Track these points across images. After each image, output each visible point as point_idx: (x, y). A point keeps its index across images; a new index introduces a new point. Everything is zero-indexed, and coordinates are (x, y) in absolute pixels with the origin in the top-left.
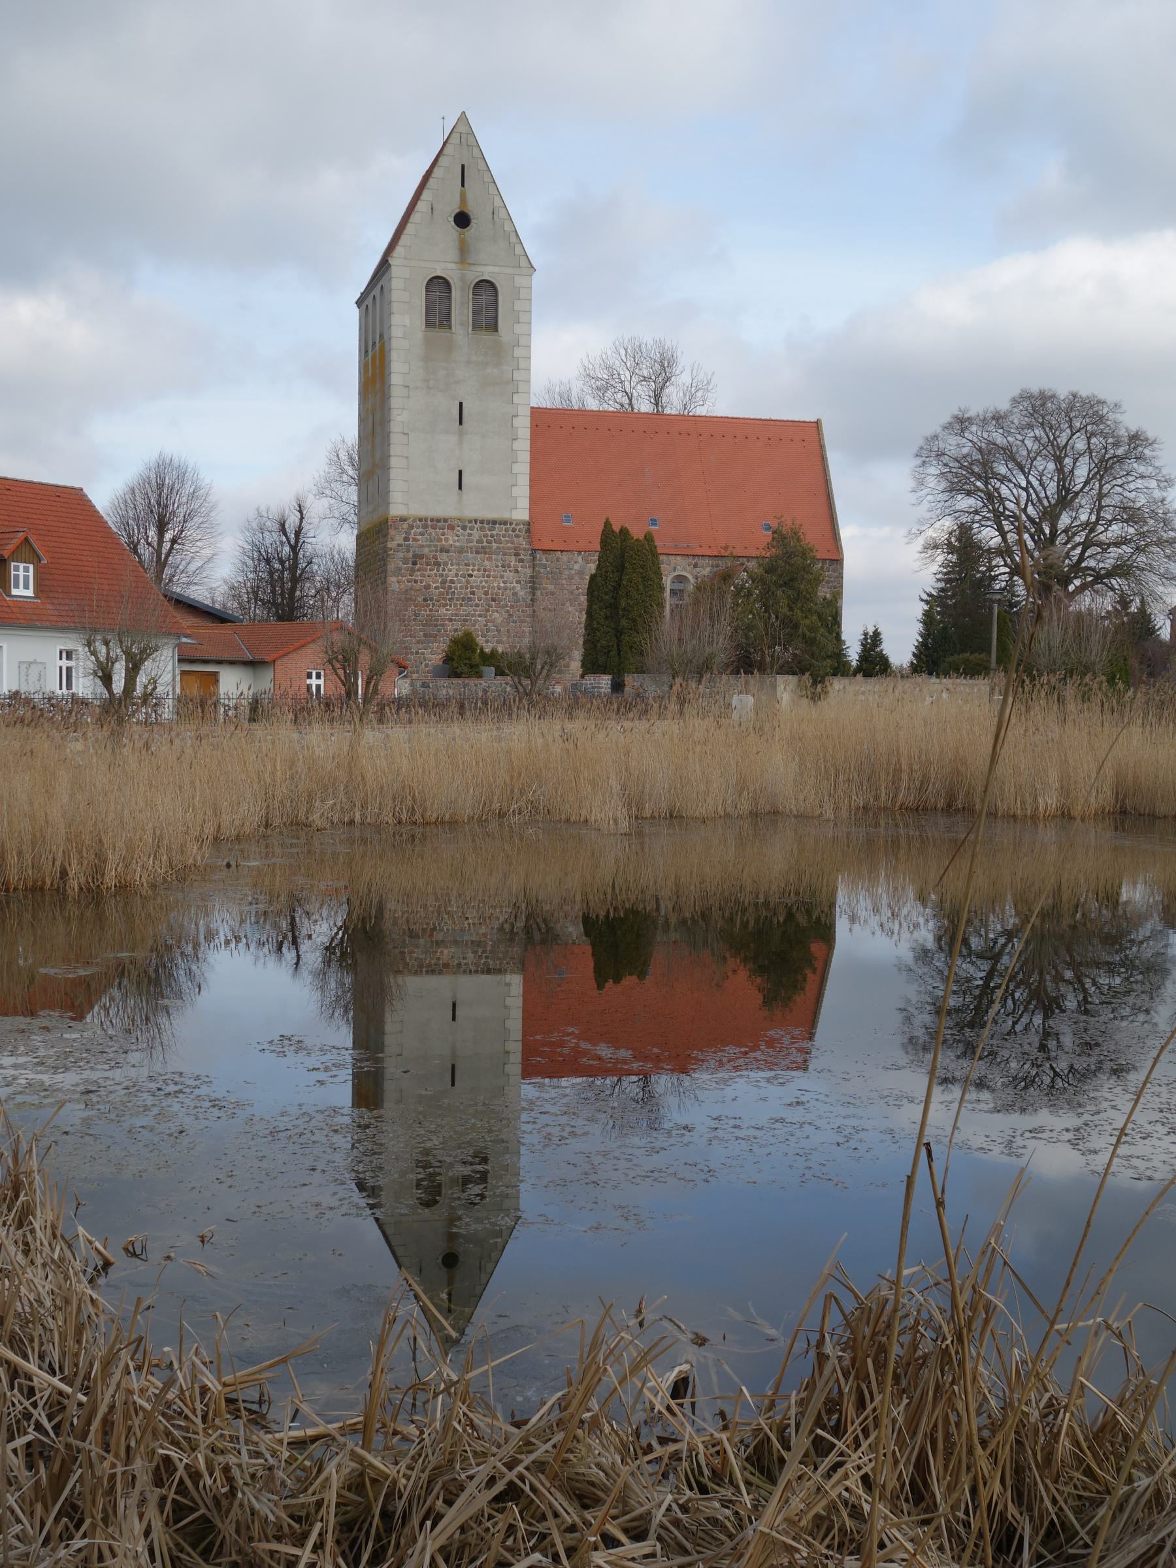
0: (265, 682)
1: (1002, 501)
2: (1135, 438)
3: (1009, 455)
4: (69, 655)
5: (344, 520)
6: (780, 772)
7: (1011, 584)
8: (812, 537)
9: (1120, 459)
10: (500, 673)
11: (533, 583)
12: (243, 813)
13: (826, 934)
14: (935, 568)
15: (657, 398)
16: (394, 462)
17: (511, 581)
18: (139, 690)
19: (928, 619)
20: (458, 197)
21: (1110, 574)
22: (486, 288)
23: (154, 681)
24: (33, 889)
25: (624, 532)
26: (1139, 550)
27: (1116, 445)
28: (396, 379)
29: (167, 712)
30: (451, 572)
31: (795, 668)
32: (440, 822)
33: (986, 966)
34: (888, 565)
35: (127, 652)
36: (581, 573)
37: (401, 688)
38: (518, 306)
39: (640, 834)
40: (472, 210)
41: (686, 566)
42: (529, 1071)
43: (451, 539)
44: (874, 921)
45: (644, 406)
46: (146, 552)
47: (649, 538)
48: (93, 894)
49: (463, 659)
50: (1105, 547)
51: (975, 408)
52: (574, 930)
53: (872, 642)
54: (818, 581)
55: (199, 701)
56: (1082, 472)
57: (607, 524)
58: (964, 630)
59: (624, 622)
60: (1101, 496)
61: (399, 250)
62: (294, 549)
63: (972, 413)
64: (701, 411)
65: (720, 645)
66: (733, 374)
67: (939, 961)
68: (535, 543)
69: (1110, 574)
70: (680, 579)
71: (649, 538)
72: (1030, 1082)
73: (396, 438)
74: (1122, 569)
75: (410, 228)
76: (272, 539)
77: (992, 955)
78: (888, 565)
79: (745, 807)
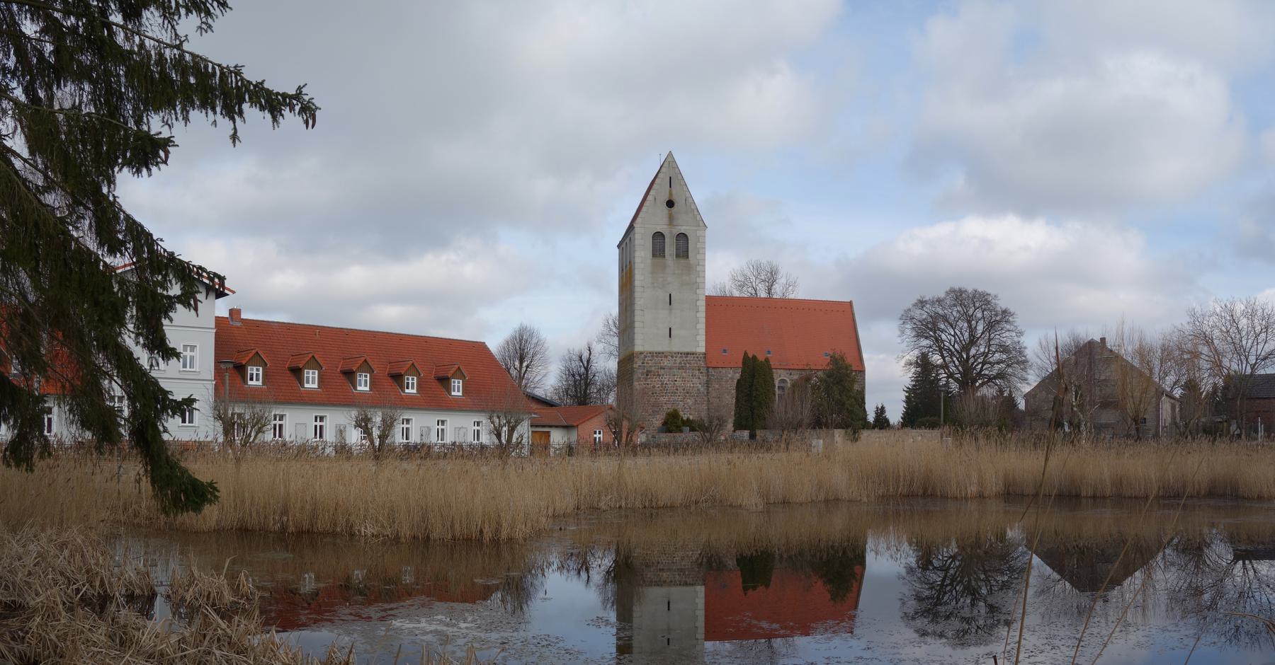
0: (574, 436)
1: (943, 341)
2: (1005, 312)
3: (945, 319)
4: (478, 424)
5: (611, 354)
6: (839, 479)
7: (947, 382)
8: (850, 359)
9: (998, 322)
10: (692, 429)
11: (708, 384)
12: (565, 503)
13: (860, 560)
14: (910, 375)
15: (769, 290)
16: (637, 324)
17: (697, 383)
18: (514, 440)
19: (908, 400)
20: (668, 192)
21: (995, 378)
22: (683, 237)
23: (521, 436)
24: (467, 540)
25: (754, 357)
26: (1008, 366)
27: (996, 315)
28: (637, 283)
29: (526, 451)
30: (666, 379)
31: (843, 425)
32: (665, 507)
33: (942, 574)
34: (887, 374)
35: (509, 422)
36: (732, 378)
37: (641, 438)
38: (699, 245)
39: (768, 512)
40: (675, 198)
41: (779, 373)
42: (707, 639)
43: (666, 363)
44: (887, 555)
45: (763, 294)
46: (514, 373)
47: (767, 360)
48: (495, 542)
49: (673, 423)
50: (992, 364)
51: (928, 297)
52: (731, 563)
53: (881, 412)
54: (854, 381)
55: (541, 444)
56: (980, 328)
57: (746, 353)
58: (926, 405)
59: (755, 404)
60: (990, 340)
61: (639, 220)
62: (586, 369)
63: (927, 298)
64: (792, 297)
65: (806, 414)
66: (806, 281)
67: (919, 573)
68: (708, 364)
69: (995, 378)
70: (783, 381)
71: (767, 360)
72: (965, 632)
73: (637, 313)
74: (1001, 375)
75: (644, 209)
76: (575, 364)
77: (945, 569)
78: (887, 374)
79: (822, 497)
